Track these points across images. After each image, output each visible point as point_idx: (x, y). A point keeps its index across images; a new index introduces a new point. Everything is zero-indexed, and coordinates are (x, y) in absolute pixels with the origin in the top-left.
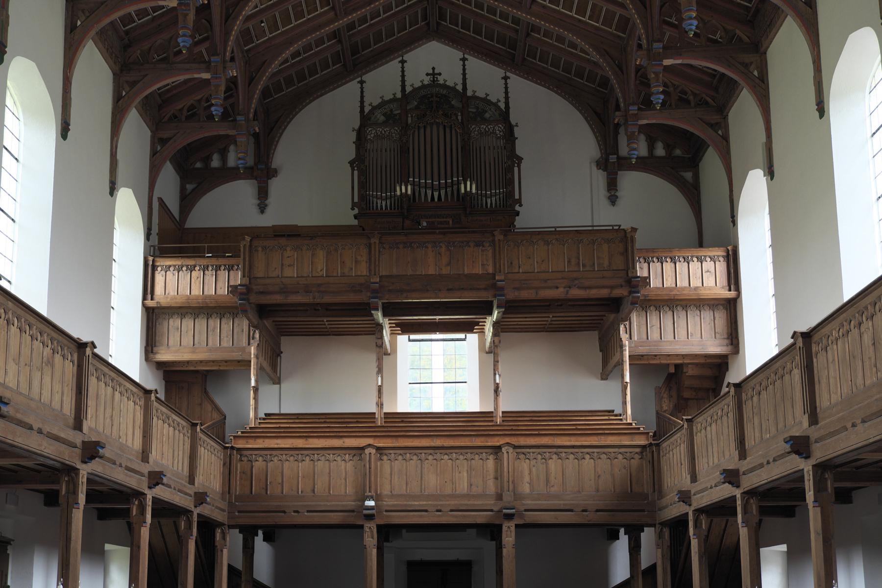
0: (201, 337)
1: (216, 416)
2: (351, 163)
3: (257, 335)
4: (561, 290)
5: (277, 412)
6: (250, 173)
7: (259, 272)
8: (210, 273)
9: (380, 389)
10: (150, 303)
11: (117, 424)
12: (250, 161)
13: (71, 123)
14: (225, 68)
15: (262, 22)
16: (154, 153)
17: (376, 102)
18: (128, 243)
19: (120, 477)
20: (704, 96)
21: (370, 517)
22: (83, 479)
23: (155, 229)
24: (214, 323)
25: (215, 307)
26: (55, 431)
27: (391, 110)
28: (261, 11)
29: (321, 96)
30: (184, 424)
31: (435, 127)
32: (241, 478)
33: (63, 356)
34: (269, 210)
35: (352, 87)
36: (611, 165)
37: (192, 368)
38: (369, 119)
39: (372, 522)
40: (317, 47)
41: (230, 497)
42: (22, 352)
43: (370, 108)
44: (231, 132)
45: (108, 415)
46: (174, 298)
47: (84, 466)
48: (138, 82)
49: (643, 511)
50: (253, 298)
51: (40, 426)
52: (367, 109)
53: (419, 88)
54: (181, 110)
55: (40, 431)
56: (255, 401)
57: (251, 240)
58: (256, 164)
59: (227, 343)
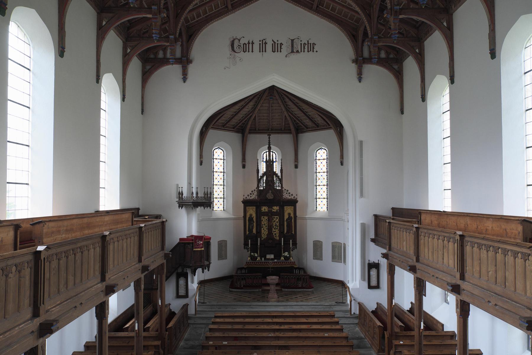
6: (178, 61)
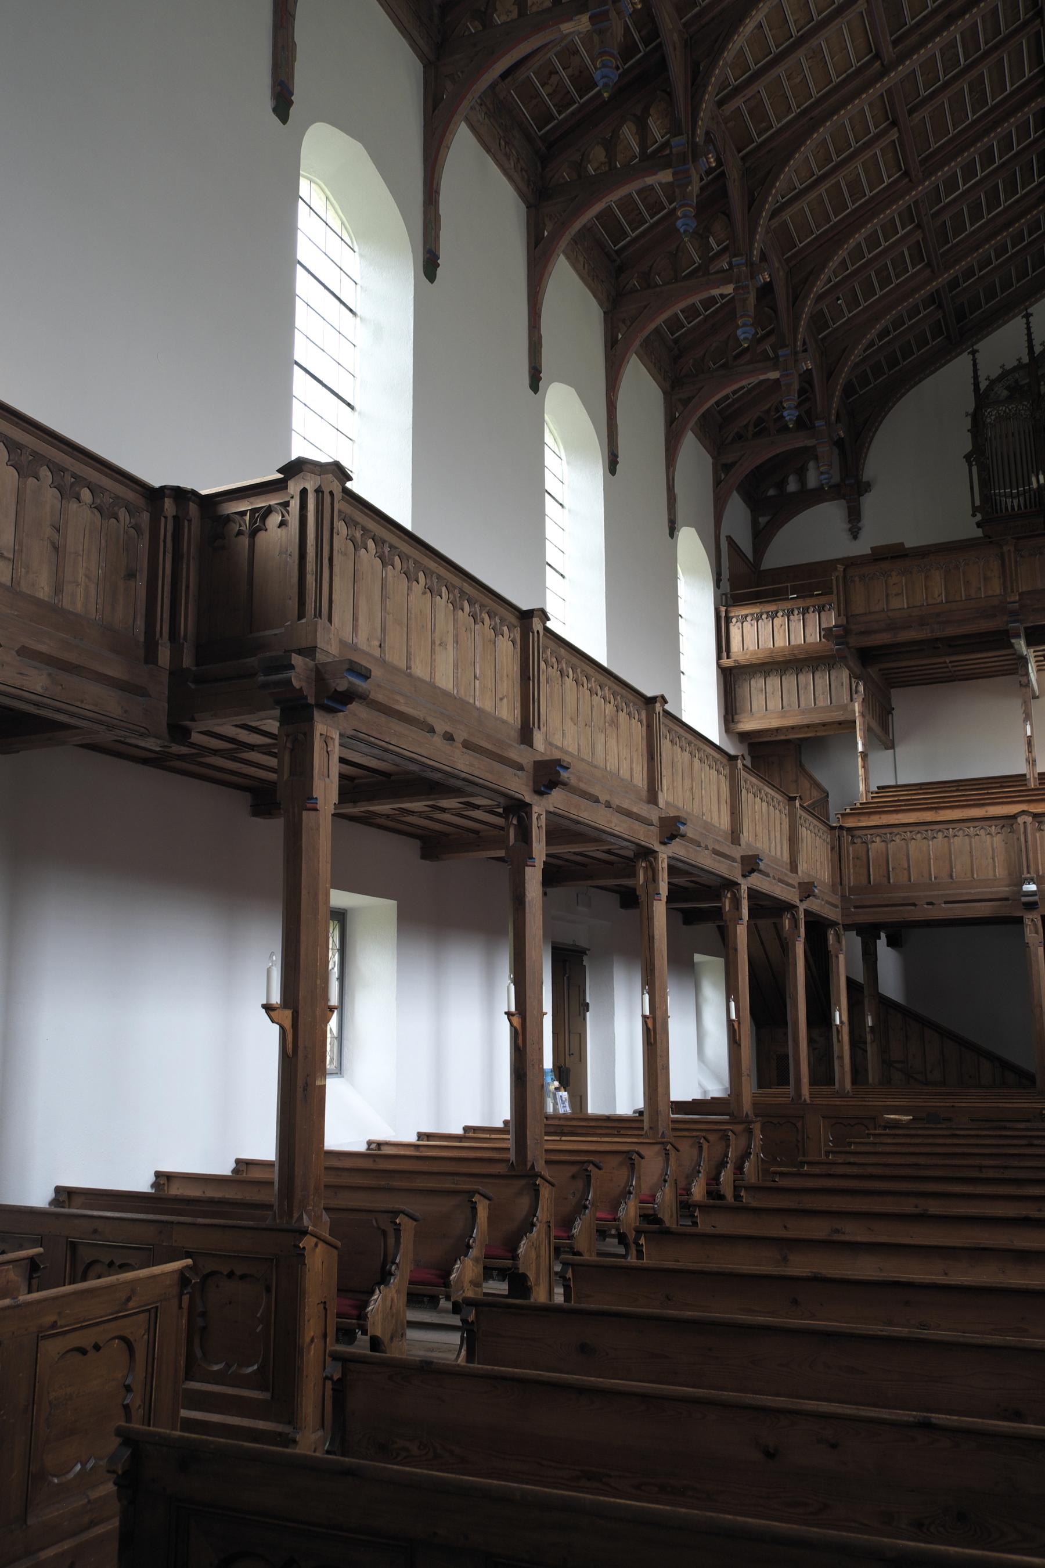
0: (791, 699)
1: (816, 795)
2: (968, 457)
3: (861, 688)
5: (893, 783)
6: (836, 492)
8: (796, 617)
9: (1029, 741)
10: (726, 662)
11: (699, 795)
12: (836, 479)
13: (620, 455)
15: (838, 299)
16: (717, 483)
17: (995, 373)
18: (696, 600)
19: (706, 860)
21: (1031, 906)
22: (663, 864)
23: (726, 574)
24: (806, 678)
25: (806, 659)
26: (626, 805)
27: (1016, 381)
28: (837, 285)
29: (920, 381)
30: (780, 798)
32: (855, 866)
33: (629, 714)
34: (863, 534)
35: (963, 361)
37: (783, 737)
39: (1035, 912)
40: (910, 320)
41: (843, 889)
42: (581, 710)
43: (987, 383)
44: (810, 443)
45: (687, 786)
46: (754, 653)
47: (663, 847)
48: (693, 397)
50: (853, 641)
51: (608, 798)
52: (983, 385)
54: (746, 426)
55: (608, 805)
56: (865, 773)
57: (844, 570)
59: (823, 701)
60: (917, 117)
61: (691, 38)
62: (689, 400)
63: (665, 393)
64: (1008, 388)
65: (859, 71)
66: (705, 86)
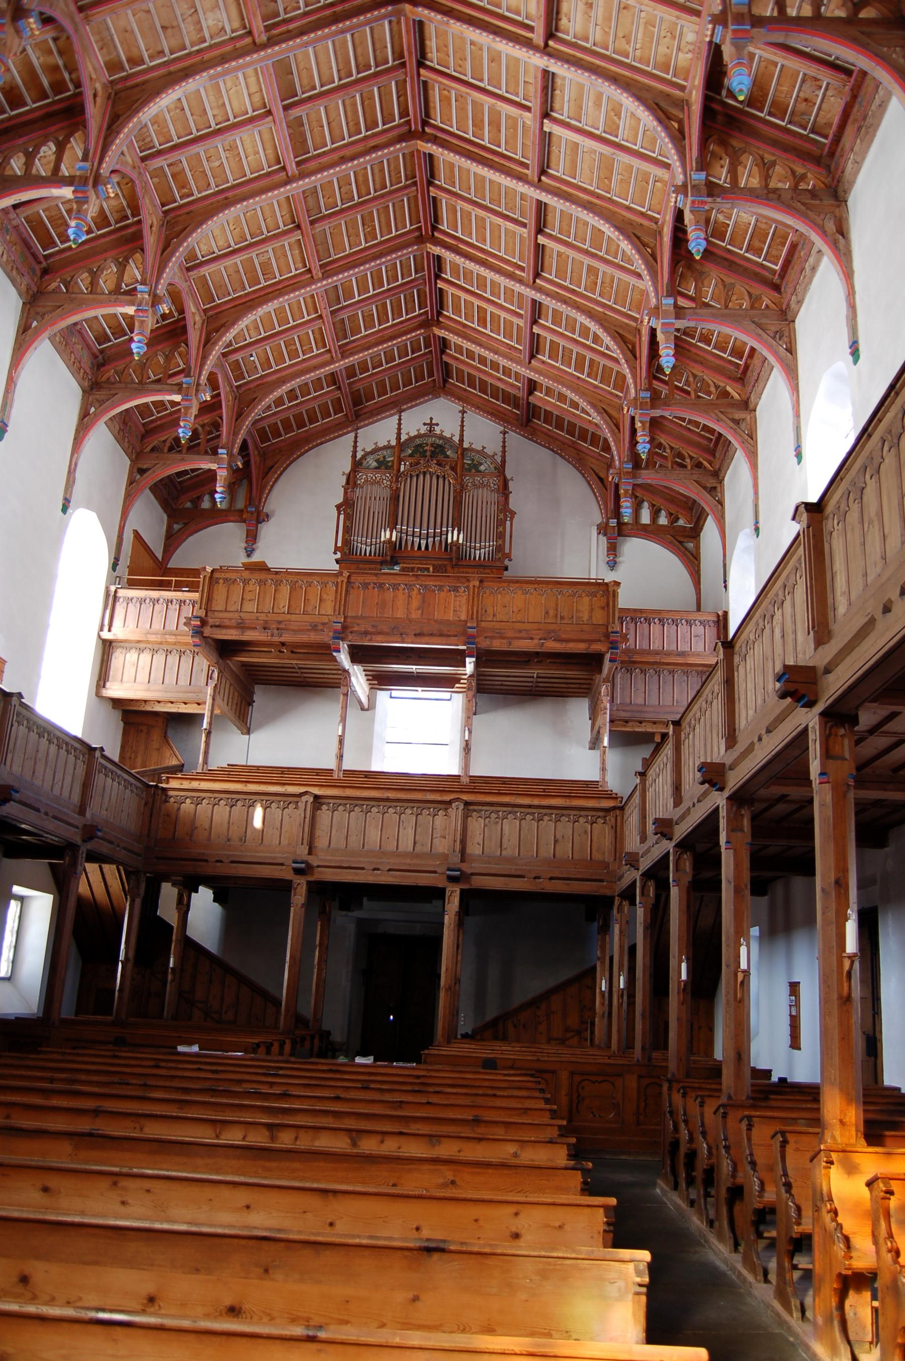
2: (338, 507)
3: (216, 675)
4: (536, 641)
7: (218, 603)
14: (197, 390)
15: (251, 356)
16: (131, 482)
20: (701, 460)
27: (384, 457)
31: (428, 476)
36: (615, 532)
38: (361, 464)
43: (363, 453)
49: (602, 881)
52: (359, 455)
53: (416, 437)
54: (164, 442)
58: (246, 507)
60: (319, 227)
61: (116, 94)
62: (103, 402)
63: (84, 391)
64: (377, 461)
65: (269, 174)
66: (118, 133)
